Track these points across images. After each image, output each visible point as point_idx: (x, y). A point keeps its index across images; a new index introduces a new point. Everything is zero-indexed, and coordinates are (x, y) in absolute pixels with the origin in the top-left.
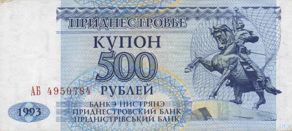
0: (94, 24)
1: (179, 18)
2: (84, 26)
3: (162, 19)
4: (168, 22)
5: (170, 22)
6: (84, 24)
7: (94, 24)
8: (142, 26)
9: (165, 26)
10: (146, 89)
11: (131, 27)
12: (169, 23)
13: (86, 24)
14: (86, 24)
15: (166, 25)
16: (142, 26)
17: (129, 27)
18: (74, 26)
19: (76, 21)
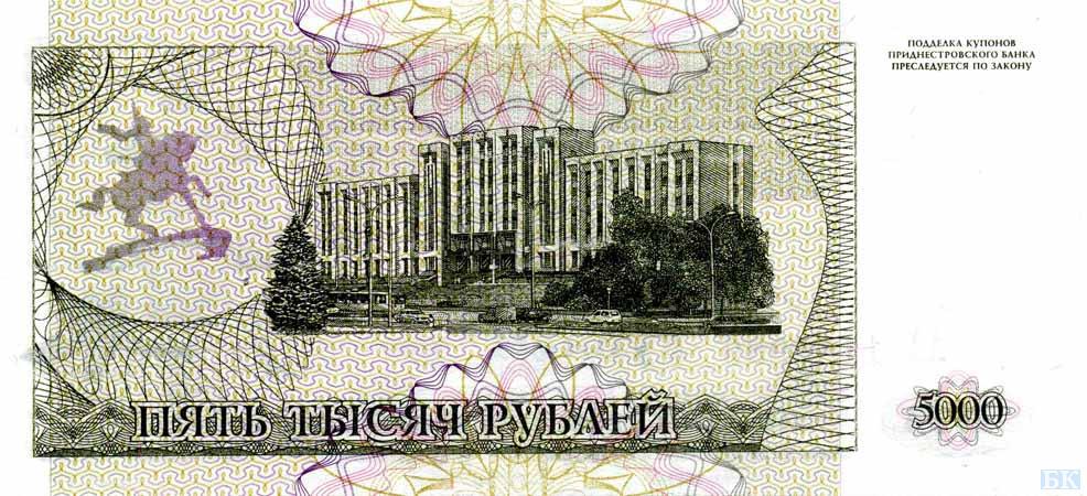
0: (654, 425)
1: (465, 437)
2: (495, 430)
3: (369, 431)
4: (187, 423)
5: (180, 424)
6: (496, 424)
7: (654, 425)
8: (426, 434)
9: (455, 408)
10: (195, 429)
11: (964, 425)
12: (184, 418)
13: (503, 423)
14: (503, 423)
15: (194, 412)
16: (426, 434)
17: (962, 423)
18: (313, 433)
19: (161, 415)
